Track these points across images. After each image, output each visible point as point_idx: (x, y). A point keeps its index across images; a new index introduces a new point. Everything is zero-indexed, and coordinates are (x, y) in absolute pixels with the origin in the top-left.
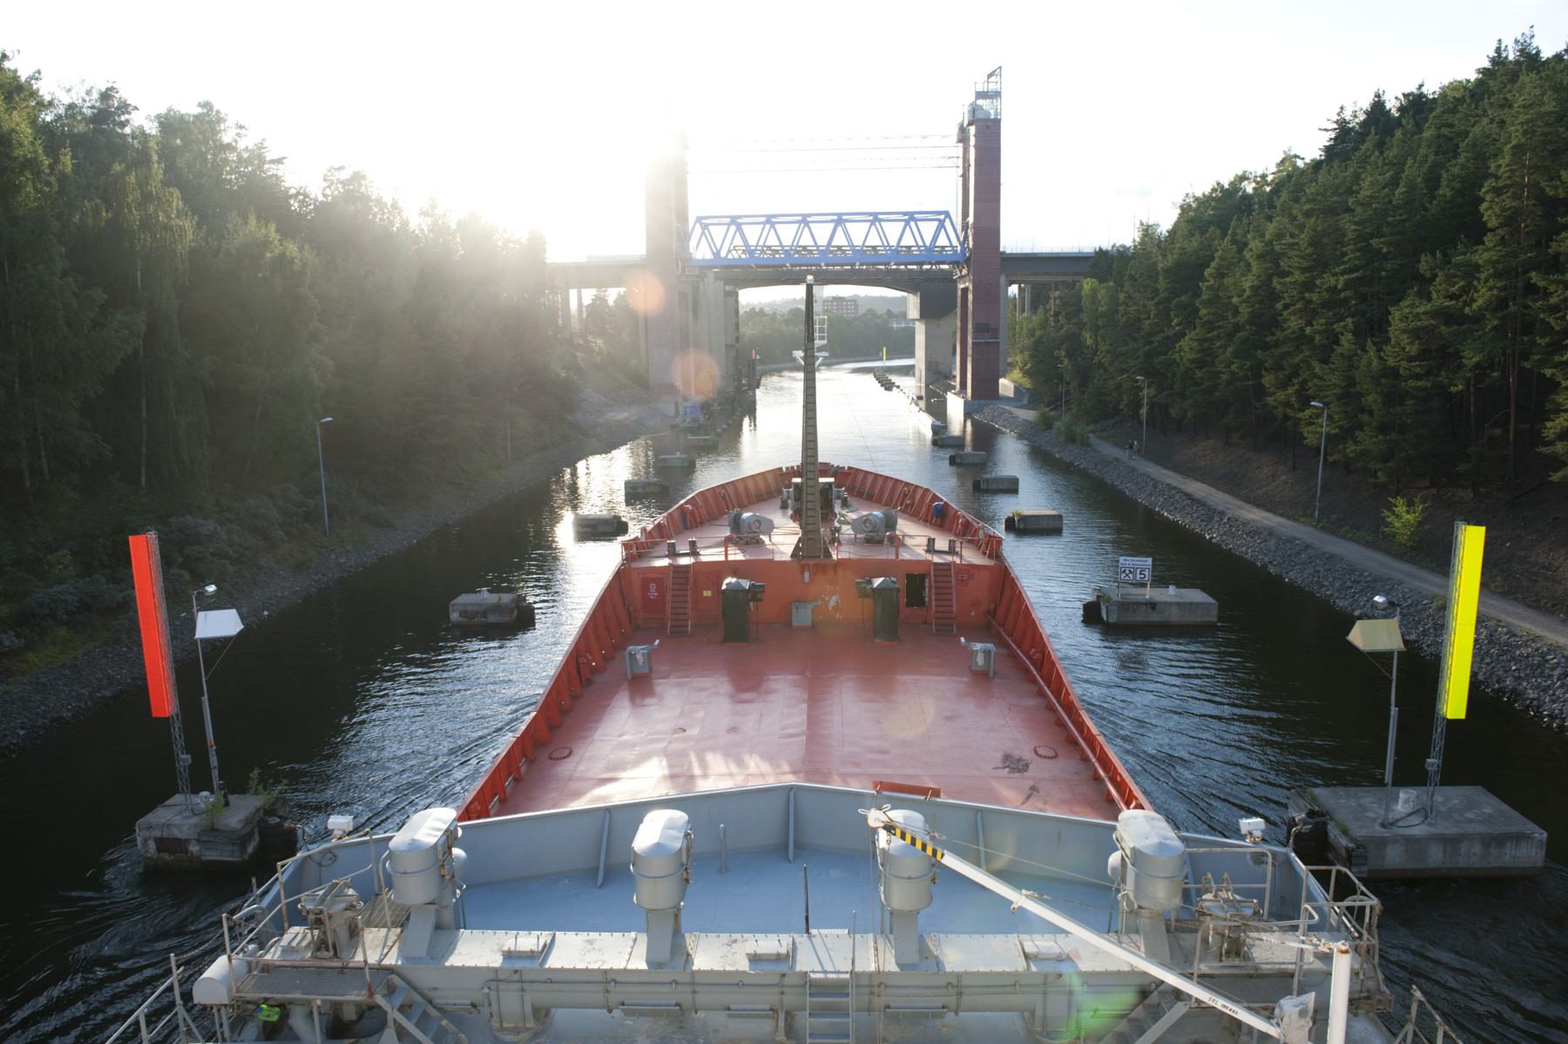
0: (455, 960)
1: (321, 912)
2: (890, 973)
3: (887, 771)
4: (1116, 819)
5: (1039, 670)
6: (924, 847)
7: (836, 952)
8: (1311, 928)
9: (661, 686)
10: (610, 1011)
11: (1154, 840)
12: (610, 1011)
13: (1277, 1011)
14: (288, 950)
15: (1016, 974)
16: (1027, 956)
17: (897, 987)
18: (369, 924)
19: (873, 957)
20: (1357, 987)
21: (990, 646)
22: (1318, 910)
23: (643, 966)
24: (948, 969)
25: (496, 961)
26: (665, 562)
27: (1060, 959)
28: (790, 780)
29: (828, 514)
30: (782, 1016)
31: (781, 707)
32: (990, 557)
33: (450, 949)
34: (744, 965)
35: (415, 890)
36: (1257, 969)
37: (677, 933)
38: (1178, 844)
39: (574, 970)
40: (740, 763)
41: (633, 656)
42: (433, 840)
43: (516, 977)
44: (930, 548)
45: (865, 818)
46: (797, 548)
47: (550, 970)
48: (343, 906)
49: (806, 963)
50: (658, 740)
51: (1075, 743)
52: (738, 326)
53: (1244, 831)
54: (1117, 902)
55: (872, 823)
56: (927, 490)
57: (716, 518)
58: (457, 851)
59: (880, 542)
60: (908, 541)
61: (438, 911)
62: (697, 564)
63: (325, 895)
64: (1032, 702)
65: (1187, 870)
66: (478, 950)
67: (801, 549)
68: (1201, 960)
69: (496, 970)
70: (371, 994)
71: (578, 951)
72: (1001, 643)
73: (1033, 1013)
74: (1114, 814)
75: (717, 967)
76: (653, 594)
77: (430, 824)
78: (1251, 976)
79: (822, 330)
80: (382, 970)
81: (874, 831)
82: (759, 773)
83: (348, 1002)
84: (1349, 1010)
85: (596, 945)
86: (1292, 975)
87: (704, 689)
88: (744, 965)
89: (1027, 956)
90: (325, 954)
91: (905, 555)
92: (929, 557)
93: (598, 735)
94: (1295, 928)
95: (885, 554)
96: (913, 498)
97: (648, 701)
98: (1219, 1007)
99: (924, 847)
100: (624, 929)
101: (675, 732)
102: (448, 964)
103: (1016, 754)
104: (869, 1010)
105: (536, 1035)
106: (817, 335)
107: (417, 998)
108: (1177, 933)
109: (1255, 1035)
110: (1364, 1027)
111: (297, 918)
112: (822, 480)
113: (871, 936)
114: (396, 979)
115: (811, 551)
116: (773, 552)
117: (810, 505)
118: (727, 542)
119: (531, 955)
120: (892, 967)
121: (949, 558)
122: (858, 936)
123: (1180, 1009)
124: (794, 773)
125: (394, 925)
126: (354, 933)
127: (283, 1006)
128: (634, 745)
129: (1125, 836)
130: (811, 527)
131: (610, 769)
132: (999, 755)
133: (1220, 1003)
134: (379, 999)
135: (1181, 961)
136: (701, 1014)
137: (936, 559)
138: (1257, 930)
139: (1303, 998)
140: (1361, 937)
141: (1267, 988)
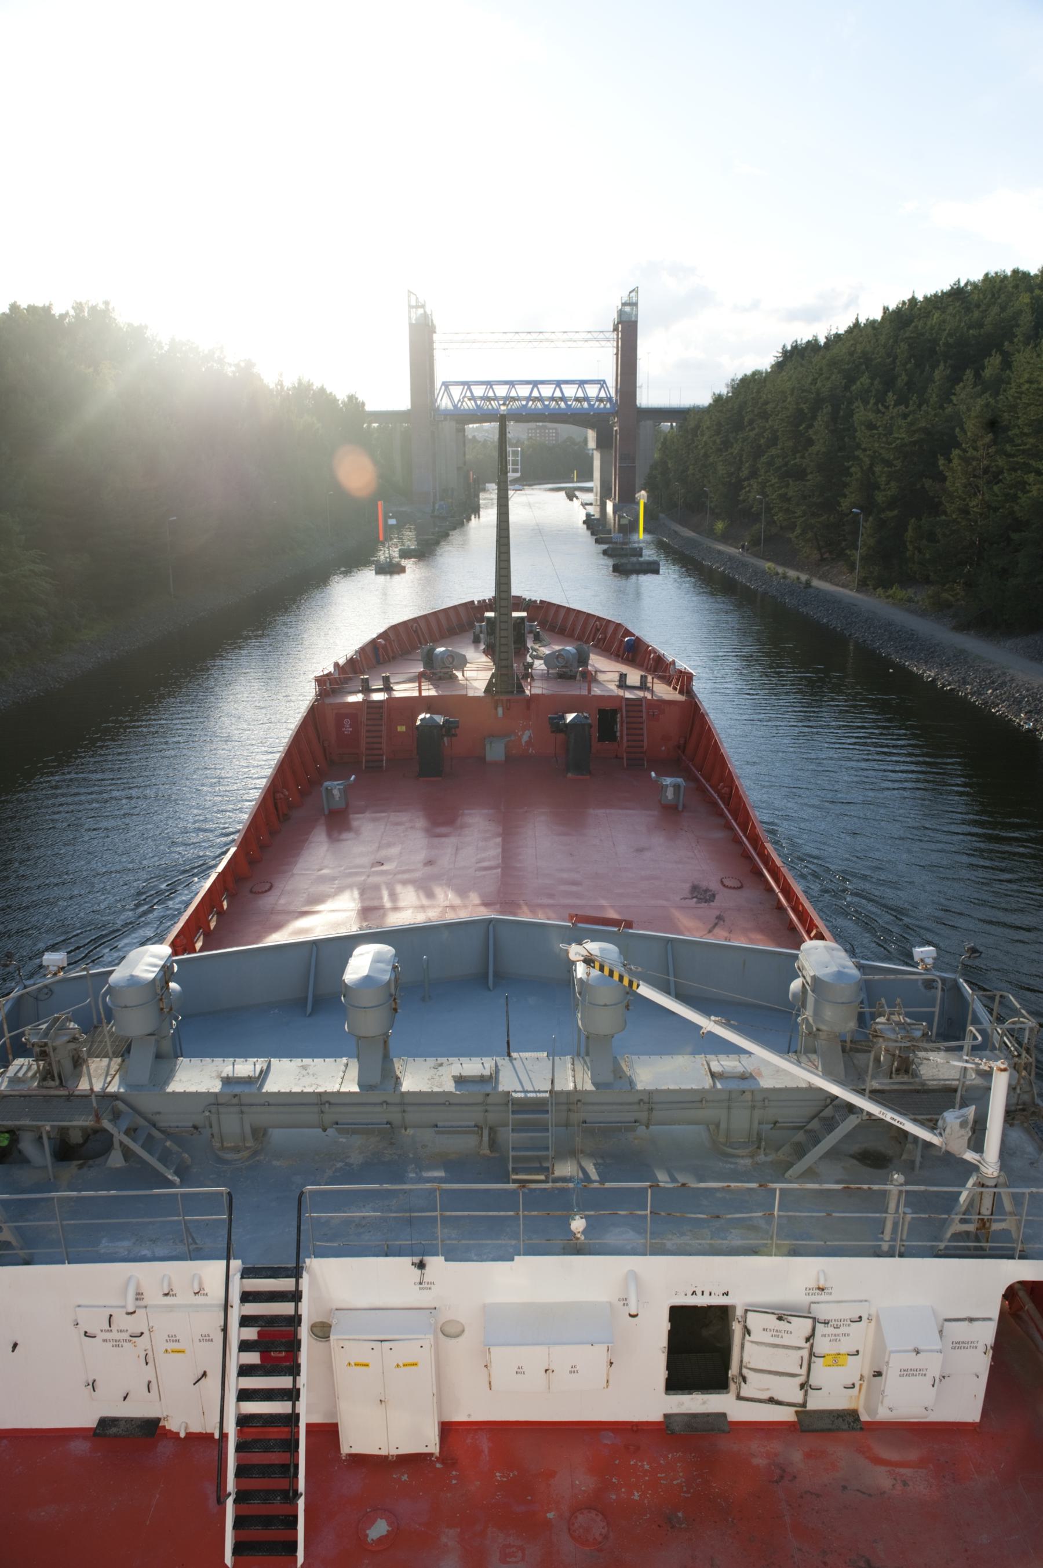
1: (46, 1044)
3: (578, 902)
4: (799, 949)
5: (727, 805)
6: (621, 978)
7: (533, 1073)
8: (975, 1049)
10: (325, 1130)
11: (833, 969)
12: (325, 1130)
13: (940, 1123)
14: (14, 1080)
15: (703, 1091)
16: (713, 1075)
17: (593, 1104)
18: (91, 1054)
19: (572, 1077)
20: (1014, 1101)
21: (679, 780)
22: (982, 1032)
23: (356, 1089)
24: (640, 1087)
25: (216, 1087)
26: (359, 698)
27: (744, 1077)
28: (484, 913)
29: (521, 649)
30: (486, 1132)
31: (476, 843)
32: (681, 692)
34: (450, 1086)
35: (136, 1023)
36: (923, 1084)
37: (387, 1060)
38: (855, 972)
39: (291, 1094)
40: (430, 895)
41: (329, 791)
42: (152, 976)
43: (235, 1101)
45: (567, 952)
48: (66, 1038)
49: (508, 1083)
50: (356, 874)
52: (445, 468)
53: (917, 958)
54: (797, 1024)
55: (572, 956)
56: (619, 625)
57: (408, 652)
58: (173, 985)
59: (572, 677)
60: (601, 677)
61: (157, 1041)
62: (391, 700)
63: (49, 1028)
64: (719, 835)
65: (863, 995)
66: (196, 1077)
67: (495, 685)
68: (873, 1077)
69: (216, 1095)
70: (98, 1119)
71: (289, 1076)
72: (689, 777)
73: (718, 1125)
74: (798, 944)
76: (348, 729)
77: (147, 960)
78: (918, 1091)
79: (515, 463)
80: (105, 1097)
81: (574, 963)
82: (469, 908)
83: (74, 1127)
84: (1006, 1121)
85: (311, 1070)
86: (955, 1090)
87: (397, 824)
88: (450, 1086)
89: (713, 1075)
90: (52, 1084)
91: (597, 691)
92: (621, 693)
94: (960, 1048)
95: (578, 690)
96: (605, 633)
97: (344, 836)
98: (888, 1119)
99: (621, 978)
100: (336, 1055)
102: (170, 1089)
103: (704, 884)
104: (567, 1125)
105: (256, 1153)
106: (510, 467)
107: (142, 1122)
108: (851, 1055)
110: (1018, 1135)
111: (22, 1050)
112: (515, 614)
113: (568, 1058)
114: (121, 1105)
115: (507, 682)
116: (466, 687)
117: (503, 641)
118: (419, 678)
119: (248, 1081)
120: (589, 1086)
121: (640, 694)
122: (557, 1058)
123: (853, 1121)
124: (485, 904)
125: (116, 1055)
126: (78, 1062)
128: (334, 878)
129: (806, 965)
130: (504, 663)
132: (687, 886)
133: (889, 1116)
134: (106, 1124)
135: (854, 1079)
136: (410, 1131)
137: (628, 695)
138: (926, 1050)
139: (964, 1111)
140: (1019, 1056)
141: (932, 1102)
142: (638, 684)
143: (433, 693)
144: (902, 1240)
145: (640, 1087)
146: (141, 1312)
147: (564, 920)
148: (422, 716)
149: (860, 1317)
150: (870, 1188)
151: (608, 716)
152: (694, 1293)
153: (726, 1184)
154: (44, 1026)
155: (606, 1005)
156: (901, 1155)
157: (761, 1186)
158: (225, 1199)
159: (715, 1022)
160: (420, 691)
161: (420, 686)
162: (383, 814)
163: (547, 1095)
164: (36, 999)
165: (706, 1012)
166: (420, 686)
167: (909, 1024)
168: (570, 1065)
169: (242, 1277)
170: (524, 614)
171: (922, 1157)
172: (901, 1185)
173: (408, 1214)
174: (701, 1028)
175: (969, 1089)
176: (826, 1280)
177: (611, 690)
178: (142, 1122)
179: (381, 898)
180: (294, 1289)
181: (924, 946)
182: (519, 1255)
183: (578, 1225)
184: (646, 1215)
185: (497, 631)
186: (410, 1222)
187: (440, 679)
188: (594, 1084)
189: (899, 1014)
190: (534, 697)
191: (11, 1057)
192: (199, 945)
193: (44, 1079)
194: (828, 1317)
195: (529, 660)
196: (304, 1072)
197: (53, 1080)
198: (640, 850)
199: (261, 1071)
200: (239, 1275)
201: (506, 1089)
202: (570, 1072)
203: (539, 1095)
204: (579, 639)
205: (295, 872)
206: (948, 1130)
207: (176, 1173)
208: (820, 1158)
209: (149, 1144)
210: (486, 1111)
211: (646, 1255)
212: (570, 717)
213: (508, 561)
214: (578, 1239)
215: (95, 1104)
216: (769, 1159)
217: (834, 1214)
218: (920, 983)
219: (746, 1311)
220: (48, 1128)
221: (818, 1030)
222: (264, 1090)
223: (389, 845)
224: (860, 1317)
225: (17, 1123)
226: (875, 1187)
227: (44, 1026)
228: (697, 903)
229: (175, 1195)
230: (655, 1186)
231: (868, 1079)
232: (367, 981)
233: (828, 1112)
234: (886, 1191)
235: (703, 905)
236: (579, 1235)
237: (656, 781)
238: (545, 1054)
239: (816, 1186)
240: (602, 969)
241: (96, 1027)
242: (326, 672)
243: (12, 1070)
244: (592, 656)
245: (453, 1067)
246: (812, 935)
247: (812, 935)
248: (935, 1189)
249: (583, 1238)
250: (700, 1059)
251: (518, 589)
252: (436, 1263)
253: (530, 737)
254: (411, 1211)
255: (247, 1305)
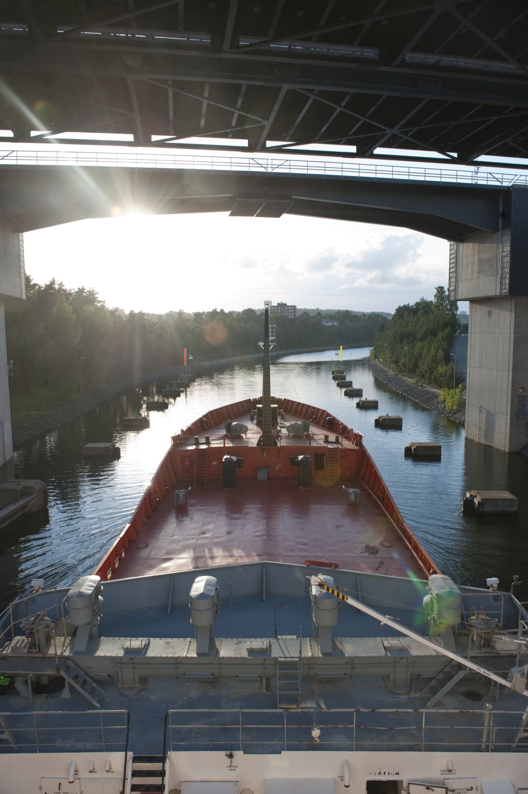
0: (100, 653)
1: (33, 629)
2: (318, 658)
5: (382, 502)
7: (290, 648)
9: (191, 510)
11: (447, 590)
13: (510, 675)
16: (385, 648)
17: (321, 664)
19: (310, 650)
21: (357, 490)
23: (195, 655)
24: (347, 655)
25: (121, 653)
26: (193, 447)
28: (256, 560)
29: (275, 423)
30: (264, 680)
31: (252, 523)
32: (356, 445)
33: (96, 648)
34: (245, 654)
35: (80, 618)
36: (498, 653)
38: (458, 591)
39: (161, 658)
42: (90, 592)
43: (131, 661)
44: (326, 440)
46: (260, 440)
47: (148, 658)
49: (276, 653)
51: (401, 540)
53: (488, 584)
60: (316, 437)
62: (210, 449)
63: (35, 620)
67: (262, 441)
70: (58, 670)
71: (159, 648)
73: (388, 677)
75: (232, 655)
78: (495, 657)
79: (272, 332)
80: (63, 658)
82: (240, 557)
83: (44, 675)
85: (171, 645)
86: (515, 656)
88: (245, 654)
89: (385, 648)
90: (34, 650)
91: (314, 444)
92: (326, 445)
93: (161, 536)
94: (516, 633)
96: (317, 415)
97: (185, 519)
98: (482, 672)
101: (200, 534)
102: (97, 655)
105: (141, 691)
106: (270, 334)
107: (81, 673)
108: (459, 636)
109: (498, 686)
111: (19, 632)
112: (272, 406)
113: (308, 639)
114: (70, 663)
115: (268, 440)
117: (266, 419)
118: (224, 438)
121: (335, 446)
123: (461, 674)
125: (68, 635)
126: (48, 639)
127: (12, 678)
129: (433, 587)
130: (267, 430)
131: (168, 553)
132: (363, 546)
133: (482, 671)
134: (63, 674)
135: (460, 650)
137: (330, 446)
142: (334, 441)
143: (231, 445)
144: (492, 742)
145: (347, 655)
146: (77, 782)
147: (303, 564)
148: (225, 457)
149: (472, 788)
150: (474, 712)
151: (320, 456)
152: (380, 773)
153: (396, 710)
154: (32, 619)
155: (328, 610)
156: (488, 693)
157: (415, 711)
158: (126, 716)
159: (388, 618)
160: (224, 444)
161: (224, 442)
162: (205, 507)
163: (298, 659)
164: (27, 604)
165: (384, 614)
166: (224, 442)
167: (488, 620)
168: (309, 643)
169: (133, 762)
170: (276, 406)
171: (499, 694)
172: (491, 710)
173: (224, 726)
174: (381, 622)
175: (522, 656)
176: (452, 766)
177: (321, 444)
178: (81, 673)
179: (205, 552)
180: (161, 769)
181: (491, 577)
182: (284, 750)
183: (316, 733)
184: (353, 728)
185: (264, 414)
186: (224, 730)
187: (234, 438)
188: (322, 653)
189: (483, 614)
190: (282, 447)
191: (13, 635)
192: (109, 576)
193: (30, 648)
194: (454, 788)
195: (279, 428)
196: (168, 646)
197: (35, 648)
198: (338, 527)
199: (145, 645)
200: (131, 761)
201: (275, 656)
202: (309, 647)
203: (293, 659)
204: (304, 417)
205: (160, 537)
206: (514, 678)
207: (98, 702)
208: (445, 695)
209: (84, 684)
210: (265, 668)
211: (353, 750)
212: (300, 457)
213: (269, 380)
214: (316, 741)
215: (57, 662)
216: (418, 695)
217: (455, 727)
218: (491, 597)
219: (409, 784)
220: (31, 675)
221: (440, 623)
222: (147, 656)
223: (209, 523)
224: (472, 788)
225: (15, 672)
226: (477, 711)
227: (32, 619)
228: (369, 554)
229: (99, 714)
230: (357, 711)
231: (469, 651)
232: (202, 596)
233: (447, 669)
234: (482, 713)
235: (372, 556)
236: (316, 739)
237: (346, 490)
238: (295, 637)
239: (445, 711)
240: (328, 589)
241: (58, 620)
242: (177, 434)
243: (14, 642)
244: (311, 427)
245: (247, 643)
246: (431, 572)
247: (431, 572)
248: (509, 712)
249: (318, 741)
250: (378, 639)
251: (275, 393)
252: (238, 754)
253: (280, 468)
254: (225, 724)
255: (135, 778)
